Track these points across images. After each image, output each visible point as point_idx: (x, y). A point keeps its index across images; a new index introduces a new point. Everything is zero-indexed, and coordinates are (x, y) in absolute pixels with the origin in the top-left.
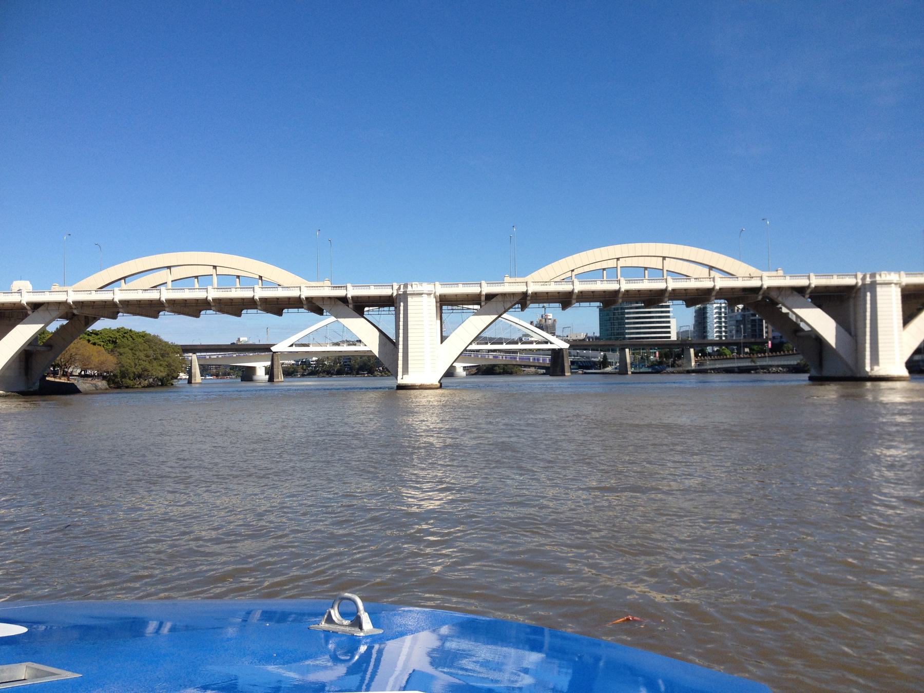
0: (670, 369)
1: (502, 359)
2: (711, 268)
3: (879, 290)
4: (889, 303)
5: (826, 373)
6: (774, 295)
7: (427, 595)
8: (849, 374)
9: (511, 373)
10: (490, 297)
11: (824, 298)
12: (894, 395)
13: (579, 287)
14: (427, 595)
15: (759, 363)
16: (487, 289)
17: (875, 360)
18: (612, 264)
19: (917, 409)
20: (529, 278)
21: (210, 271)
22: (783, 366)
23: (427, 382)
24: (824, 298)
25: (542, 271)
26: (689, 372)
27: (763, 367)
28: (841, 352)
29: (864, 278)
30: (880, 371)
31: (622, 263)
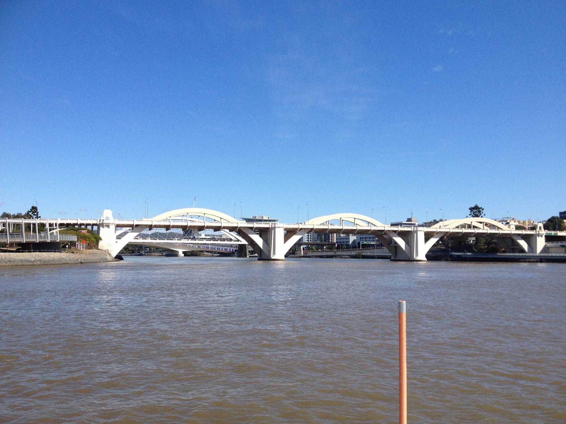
0: (292, 256)
1: (196, 248)
2: (369, 223)
3: (418, 232)
4: (421, 236)
5: (398, 258)
6: (387, 232)
7: (387, 337)
8: (408, 259)
9: (196, 255)
10: (137, 226)
11: (402, 234)
12: (281, 265)
13: (172, 224)
14: (387, 337)
15: (338, 253)
16: (136, 223)
17: (417, 255)
18: (203, 215)
19: (288, 270)
20: (153, 219)
21: (203, 215)
22: (348, 255)
23: (280, 258)
24: (402, 234)
25: (158, 216)
26: (301, 257)
27: (339, 256)
28: (406, 252)
29: (100, 221)
30: (418, 258)
31: (206, 215)
